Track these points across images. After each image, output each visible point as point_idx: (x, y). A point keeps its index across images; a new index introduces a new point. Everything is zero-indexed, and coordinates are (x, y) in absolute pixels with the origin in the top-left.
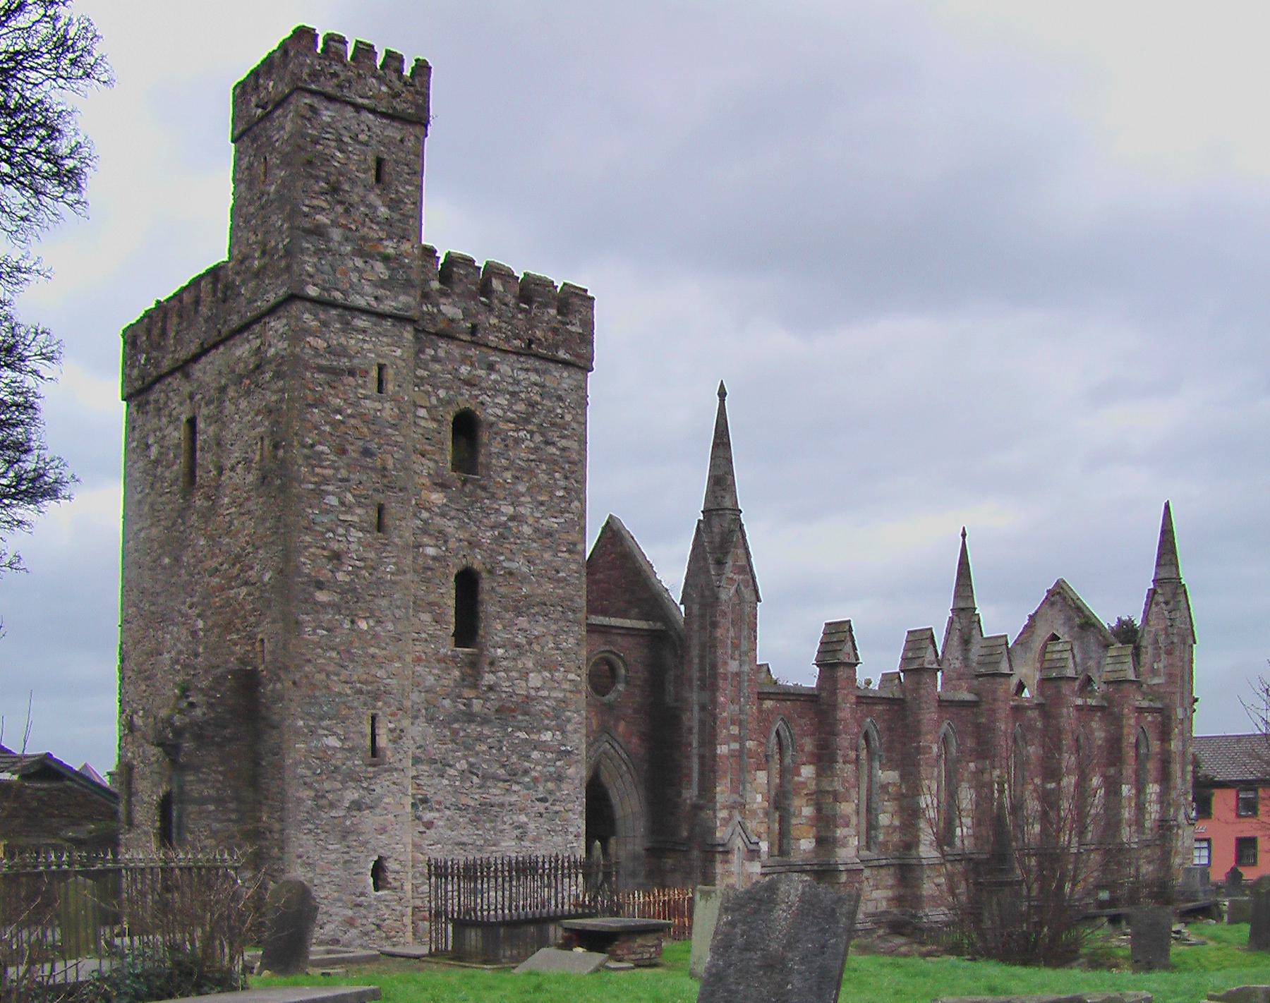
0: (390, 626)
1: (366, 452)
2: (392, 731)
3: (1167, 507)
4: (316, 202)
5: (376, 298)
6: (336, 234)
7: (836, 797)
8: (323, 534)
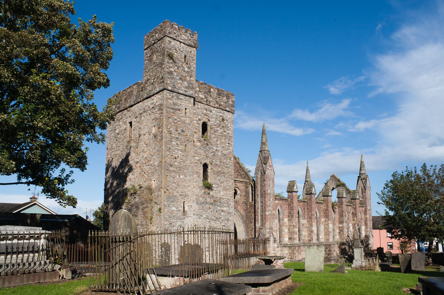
0: (188, 178)
1: (183, 131)
2: (189, 206)
4: (170, 65)
5: (185, 91)
6: (175, 74)
8: (172, 152)
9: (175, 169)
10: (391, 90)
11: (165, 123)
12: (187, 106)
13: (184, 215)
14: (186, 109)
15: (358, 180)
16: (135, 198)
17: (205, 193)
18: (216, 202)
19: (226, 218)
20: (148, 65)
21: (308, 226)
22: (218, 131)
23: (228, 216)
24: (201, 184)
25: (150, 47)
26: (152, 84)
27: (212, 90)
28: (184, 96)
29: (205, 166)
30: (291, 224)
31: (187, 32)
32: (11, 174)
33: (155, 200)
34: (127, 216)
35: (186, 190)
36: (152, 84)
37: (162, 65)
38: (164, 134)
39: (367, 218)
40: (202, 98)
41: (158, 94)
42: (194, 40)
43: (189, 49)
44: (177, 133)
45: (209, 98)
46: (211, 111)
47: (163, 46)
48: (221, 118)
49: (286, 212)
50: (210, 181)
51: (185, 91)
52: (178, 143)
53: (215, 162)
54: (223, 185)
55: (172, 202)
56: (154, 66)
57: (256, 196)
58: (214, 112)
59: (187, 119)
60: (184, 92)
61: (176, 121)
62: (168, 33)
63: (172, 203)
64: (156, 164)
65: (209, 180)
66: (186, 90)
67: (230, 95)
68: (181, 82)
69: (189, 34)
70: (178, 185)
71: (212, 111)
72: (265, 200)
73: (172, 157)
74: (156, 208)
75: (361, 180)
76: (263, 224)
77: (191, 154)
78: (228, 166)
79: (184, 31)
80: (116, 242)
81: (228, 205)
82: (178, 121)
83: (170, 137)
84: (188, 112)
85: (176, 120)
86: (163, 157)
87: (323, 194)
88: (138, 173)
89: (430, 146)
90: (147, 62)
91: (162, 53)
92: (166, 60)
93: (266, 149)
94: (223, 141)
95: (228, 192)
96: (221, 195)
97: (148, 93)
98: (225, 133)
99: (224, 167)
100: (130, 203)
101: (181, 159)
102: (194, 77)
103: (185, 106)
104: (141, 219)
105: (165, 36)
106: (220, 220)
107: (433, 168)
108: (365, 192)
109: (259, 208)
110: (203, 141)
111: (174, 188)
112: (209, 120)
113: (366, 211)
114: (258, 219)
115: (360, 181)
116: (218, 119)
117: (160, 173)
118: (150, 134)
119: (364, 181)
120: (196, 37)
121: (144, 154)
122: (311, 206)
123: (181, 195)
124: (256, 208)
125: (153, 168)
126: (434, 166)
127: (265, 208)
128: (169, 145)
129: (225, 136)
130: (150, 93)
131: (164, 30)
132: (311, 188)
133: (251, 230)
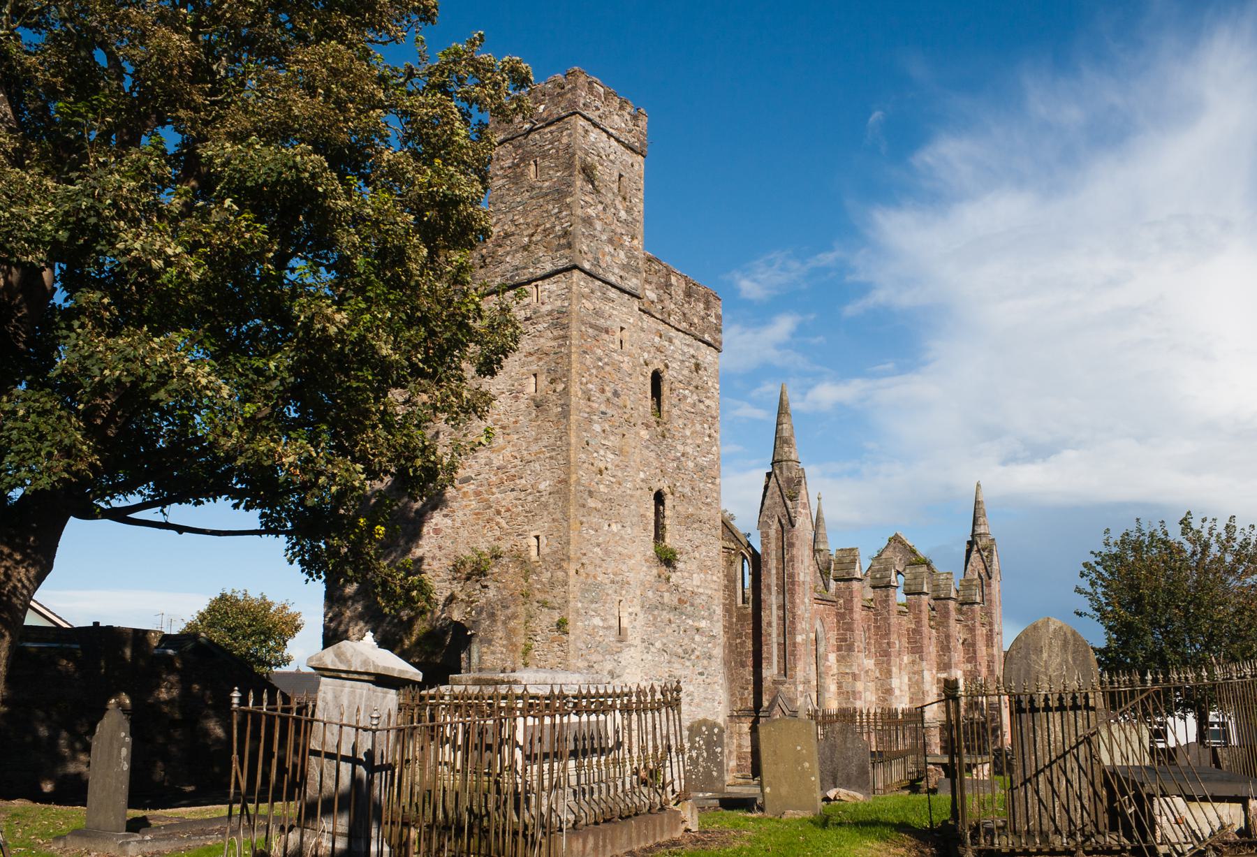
0: (629, 531)
1: (616, 394)
2: (630, 614)
3: (978, 485)
4: (587, 199)
5: (621, 277)
6: (598, 225)
7: (855, 677)
8: (592, 454)
9: (599, 505)
10: (906, 299)
11: (576, 366)
12: (625, 322)
13: (621, 641)
14: (622, 329)
15: (969, 552)
16: (486, 587)
17: (660, 577)
18: (683, 604)
19: (706, 650)
20: (504, 192)
21: (878, 675)
22: (685, 397)
23: (710, 645)
24: (651, 552)
25: (512, 139)
26: (525, 248)
27: (673, 279)
28: (618, 292)
29: (659, 498)
30: (848, 671)
31: (624, 109)
32: (202, 503)
33: (539, 596)
34: (1069, 635)
35: (624, 568)
36: (525, 248)
37: (566, 197)
38: (573, 399)
39: (993, 656)
40: (653, 302)
41: (547, 281)
42: (641, 133)
43: (629, 157)
44: (603, 398)
45: (667, 303)
46: (670, 341)
47: (565, 140)
48: (693, 361)
49: (833, 636)
50: (670, 541)
51: (621, 277)
52: (607, 427)
53: (680, 489)
54: (697, 556)
55: (592, 602)
56: (532, 198)
57: (764, 591)
58: (676, 341)
59: (626, 359)
60: (619, 280)
61: (600, 364)
62: (581, 105)
63: (594, 606)
64: (542, 487)
65: (667, 540)
66: (622, 273)
67: (711, 299)
68: (612, 251)
69: (629, 114)
70: (607, 552)
71: (674, 340)
72: (793, 603)
73: (594, 469)
74: (546, 619)
75: (978, 551)
76: (785, 670)
77: (635, 461)
78: (709, 500)
79: (616, 103)
80: (1034, 710)
81: (710, 615)
82: (606, 364)
83: (587, 410)
84: (627, 338)
85: (600, 360)
86: (572, 468)
87: (907, 588)
88: (468, 513)
89: (1004, 463)
90: (501, 182)
91: (561, 160)
92: (579, 183)
93: (793, 457)
94: (698, 427)
95: (709, 577)
96: (695, 583)
97: (509, 275)
98: (702, 406)
99: (700, 505)
100: (472, 602)
101: (614, 476)
102: (639, 237)
103: (621, 321)
104: (502, 653)
105: (574, 114)
106: (693, 657)
107: (1207, 525)
108: (989, 585)
109: (774, 624)
110: (655, 425)
111: (598, 562)
112: (667, 366)
113: (991, 635)
114: (771, 654)
115: (974, 555)
116: (687, 364)
117: (558, 515)
118: (516, 397)
119: (986, 554)
120: (643, 123)
121: (493, 456)
122: (886, 619)
123: (612, 582)
124: (764, 625)
125: (530, 498)
126: (1210, 520)
127: (793, 623)
128: (585, 434)
129: (702, 414)
130: (518, 275)
131: (569, 95)
132: (886, 569)
133: (742, 688)
